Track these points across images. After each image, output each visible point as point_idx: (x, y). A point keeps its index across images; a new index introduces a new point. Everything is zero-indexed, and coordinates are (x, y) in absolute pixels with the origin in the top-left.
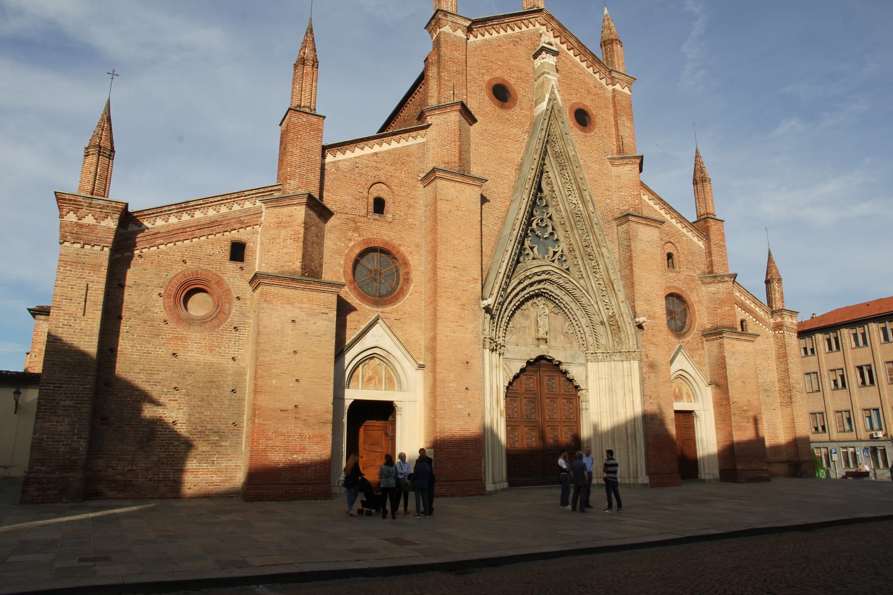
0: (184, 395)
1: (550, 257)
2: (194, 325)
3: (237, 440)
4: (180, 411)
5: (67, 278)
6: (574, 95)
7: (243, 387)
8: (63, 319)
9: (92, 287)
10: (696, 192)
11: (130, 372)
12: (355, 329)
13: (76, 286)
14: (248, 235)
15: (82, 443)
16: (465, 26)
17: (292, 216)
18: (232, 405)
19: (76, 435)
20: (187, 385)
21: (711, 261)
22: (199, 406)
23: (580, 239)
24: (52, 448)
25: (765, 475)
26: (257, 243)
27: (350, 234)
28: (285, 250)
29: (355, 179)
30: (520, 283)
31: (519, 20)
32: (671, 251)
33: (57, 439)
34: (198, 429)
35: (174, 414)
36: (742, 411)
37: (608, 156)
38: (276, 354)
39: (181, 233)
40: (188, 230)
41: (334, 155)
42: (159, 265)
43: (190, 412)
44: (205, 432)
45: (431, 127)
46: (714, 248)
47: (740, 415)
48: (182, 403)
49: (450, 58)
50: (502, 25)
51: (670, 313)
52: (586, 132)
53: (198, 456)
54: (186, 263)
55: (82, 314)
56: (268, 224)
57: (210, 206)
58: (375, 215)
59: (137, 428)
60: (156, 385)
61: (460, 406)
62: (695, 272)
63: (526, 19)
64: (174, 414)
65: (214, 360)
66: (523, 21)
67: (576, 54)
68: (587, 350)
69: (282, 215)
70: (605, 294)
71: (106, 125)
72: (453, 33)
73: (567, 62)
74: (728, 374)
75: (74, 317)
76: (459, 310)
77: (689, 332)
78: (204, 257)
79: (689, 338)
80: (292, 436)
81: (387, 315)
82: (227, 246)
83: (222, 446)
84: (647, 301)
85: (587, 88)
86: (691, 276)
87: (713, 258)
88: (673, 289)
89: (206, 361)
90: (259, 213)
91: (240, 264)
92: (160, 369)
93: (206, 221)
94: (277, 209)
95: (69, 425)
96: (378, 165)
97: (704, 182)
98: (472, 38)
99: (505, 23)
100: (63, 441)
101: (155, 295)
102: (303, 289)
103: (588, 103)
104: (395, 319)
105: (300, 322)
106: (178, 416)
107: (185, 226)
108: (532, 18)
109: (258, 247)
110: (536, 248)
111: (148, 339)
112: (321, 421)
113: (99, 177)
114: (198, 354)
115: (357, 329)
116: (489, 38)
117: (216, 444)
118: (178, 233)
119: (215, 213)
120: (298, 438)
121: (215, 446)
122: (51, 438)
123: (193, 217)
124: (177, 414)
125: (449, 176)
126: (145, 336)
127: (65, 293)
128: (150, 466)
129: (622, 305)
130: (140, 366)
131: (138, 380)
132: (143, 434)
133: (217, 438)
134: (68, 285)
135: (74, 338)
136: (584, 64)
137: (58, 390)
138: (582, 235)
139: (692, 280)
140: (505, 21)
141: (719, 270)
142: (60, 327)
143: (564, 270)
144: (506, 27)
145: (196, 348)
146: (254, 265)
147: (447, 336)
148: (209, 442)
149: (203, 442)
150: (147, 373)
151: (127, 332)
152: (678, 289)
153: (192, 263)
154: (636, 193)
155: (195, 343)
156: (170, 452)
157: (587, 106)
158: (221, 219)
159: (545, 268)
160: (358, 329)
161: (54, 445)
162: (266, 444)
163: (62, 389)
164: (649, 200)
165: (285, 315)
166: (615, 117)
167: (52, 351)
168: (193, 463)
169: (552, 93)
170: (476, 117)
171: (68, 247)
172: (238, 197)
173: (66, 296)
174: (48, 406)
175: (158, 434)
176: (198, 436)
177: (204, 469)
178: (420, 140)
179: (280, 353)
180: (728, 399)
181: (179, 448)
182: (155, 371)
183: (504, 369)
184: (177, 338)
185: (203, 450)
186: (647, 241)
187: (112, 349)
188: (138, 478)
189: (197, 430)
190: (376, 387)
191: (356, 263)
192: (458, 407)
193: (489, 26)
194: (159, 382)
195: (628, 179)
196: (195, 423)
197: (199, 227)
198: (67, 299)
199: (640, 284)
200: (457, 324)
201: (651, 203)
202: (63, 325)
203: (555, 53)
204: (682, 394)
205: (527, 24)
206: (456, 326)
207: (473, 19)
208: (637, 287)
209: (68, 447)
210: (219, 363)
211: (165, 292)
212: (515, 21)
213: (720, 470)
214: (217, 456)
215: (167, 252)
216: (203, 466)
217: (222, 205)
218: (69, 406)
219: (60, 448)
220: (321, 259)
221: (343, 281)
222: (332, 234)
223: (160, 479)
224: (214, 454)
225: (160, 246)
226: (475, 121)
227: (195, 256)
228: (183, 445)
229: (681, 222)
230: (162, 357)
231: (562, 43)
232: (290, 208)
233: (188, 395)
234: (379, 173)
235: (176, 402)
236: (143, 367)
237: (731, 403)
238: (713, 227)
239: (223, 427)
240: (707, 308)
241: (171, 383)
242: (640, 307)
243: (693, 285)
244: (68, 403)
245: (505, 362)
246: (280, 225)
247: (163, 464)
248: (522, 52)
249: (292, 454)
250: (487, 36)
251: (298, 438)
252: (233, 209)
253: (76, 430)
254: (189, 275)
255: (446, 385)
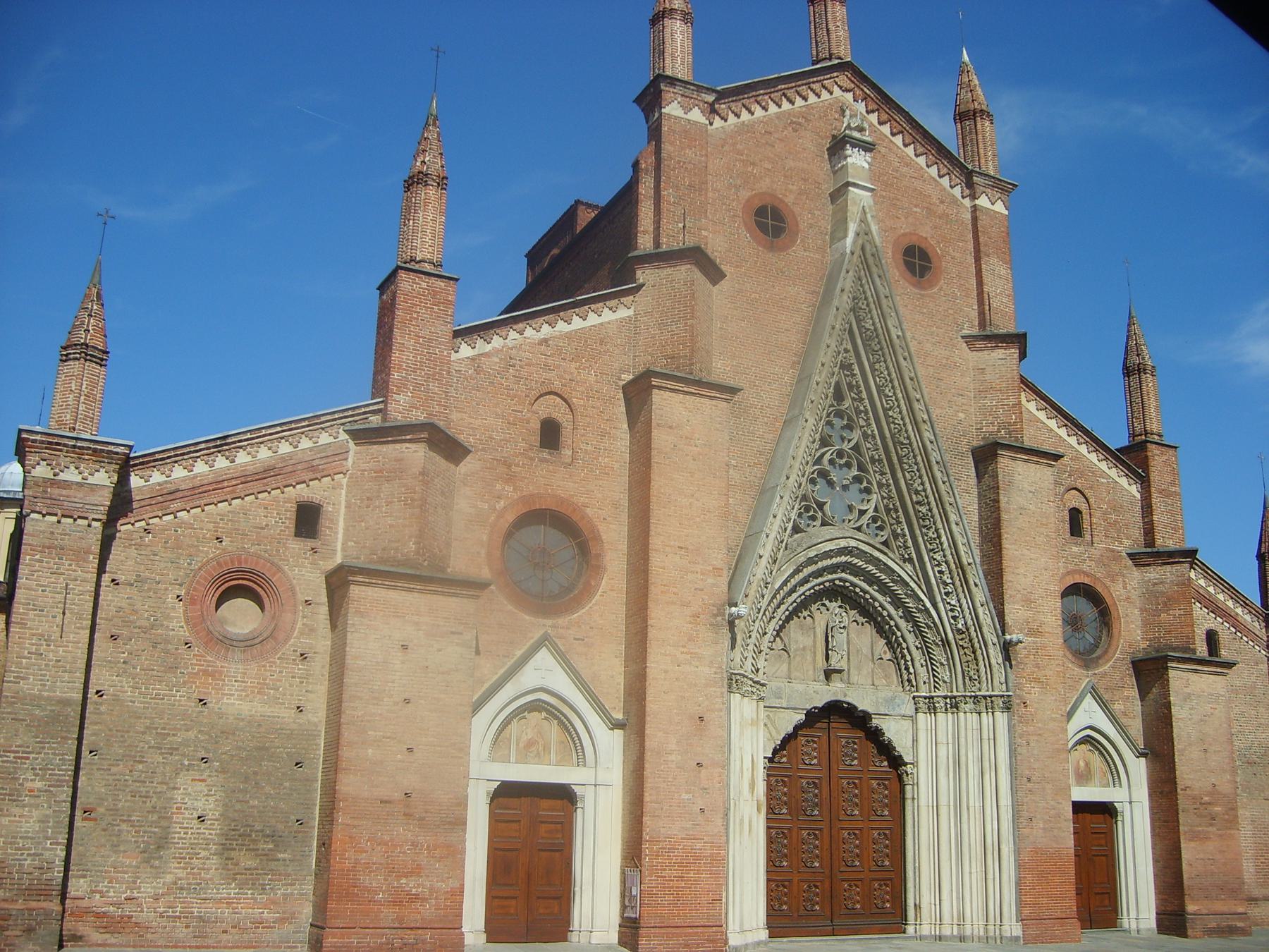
0: (216, 771)
1: (852, 522)
2: (234, 651)
3: (303, 849)
4: (211, 799)
5: (36, 574)
6: (903, 219)
7: (314, 758)
8: (29, 644)
9: (74, 589)
10: (1129, 391)
11: (128, 732)
12: (505, 656)
13: (50, 587)
14: (324, 491)
15: (59, 852)
16: (706, 103)
17: (402, 460)
18: (295, 790)
19: (48, 838)
20: (222, 754)
21: (1152, 522)
22: (241, 791)
23: (909, 490)
24: (12, 860)
25: (1240, 924)
26: (340, 504)
27: (498, 487)
28: (389, 521)
29: (508, 388)
30: (797, 571)
31: (803, 85)
32: (1076, 505)
33: (21, 845)
34: (239, 830)
35: (199, 804)
36: (1200, 803)
37: (964, 331)
38: (374, 704)
39: (213, 490)
40: (226, 484)
41: (473, 345)
42: (178, 546)
43: (227, 800)
44: (250, 836)
45: (644, 288)
46: (1156, 499)
47: (1195, 811)
48: (212, 786)
49: (679, 162)
50: (772, 96)
51: (1072, 622)
52: (923, 288)
53: (238, 876)
54: (221, 542)
55: (58, 634)
56: (359, 473)
57: (261, 443)
58: (542, 452)
59: (141, 826)
60: (171, 754)
61: (685, 796)
62: (1121, 543)
63: (817, 81)
64: (199, 804)
65: (267, 710)
66: (812, 85)
67: (907, 141)
68: (917, 691)
69: (384, 458)
70: (950, 590)
71: (95, 307)
72: (685, 116)
73: (892, 158)
74: (1175, 736)
75: (45, 640)
76: (688, 625)
77: (1106, 657)
78: (251, 532)
79: (1106, 668)
80: (399, 845)
81: (561, 631)
82: (290, 511)
83: (278, 860)
84: (1028, 602)
85: (927, 205)
86: (1113, 551)
87: (1155, 518)
88: (1078, 576)
89: (253, 713)
90: (343, 454)
91: (310, 543)
92: (178, 726)
93: (254, 468)
94: (375, 446)
95: (39, 821)
96: (550, 362)
97: (1142, 374)
98: (718, 122)
99: (777, 91)
100: (30, 849)
101: (171, 598)
102: (420, 591)
103: (927, 233)
104: (575, 639)
105: (415, 648)
106: (207, 807)
107: (221, 479)
108: (827, 79)
109: (343, 510)
110: (828, 504)
111: (159, 674)
112: (448, 820)
113: (85, 399)
114: (241, 700)
115: (508, 657)
116: (749, 121)
117: (268, 857)
118: (209, 491)
119: (270, 453)
120: (408, 849)
121: (267, 860)
122: (11, 843)
123: (233, 461)
124: (204, 804)
125: (674, 385)
126: (153, 670)
127: (33, 600)
128: (161, 891)
129: (980, 610)
130: (146, 721)
131: (142, 744)
132: (151, 837)
133: (271, 846)
134: (37, 585)
135: (45, 675)
136: (922, 161)
137: (21, 763)
138: (911, 482)
139: (1115, 556)
140: (779, 87)
141: (1166, 540)
142: (25, 658)
143: (878, 546)
144: (781, 99)
145: (237, 690)
146: (333, 544)
147: (666, 672)
148: (257, 852)
149: (247, 853)
150: (157, 733)
151: (124, 662)
152: (1088, 576)
153: (231, 542)
154: (1012, 401)
155: (235, 681)
156: (192, 869)
157: (926, 239)
158: (280, 465)
159: (843, 543)
160: (511, 656)
161: (17, 854)
162: (356, 859)
163: (27, 761)
164: (1038, 410)
165: (390, 636)
166: (978, 259)
167: (12, 697)
168: (231, 889)
169: (863, 221)
170: (723, 268)
171: (37, 520)
172: (308, 426)
173: (33, 605)
174: (6, 789)
175: (175, 838)
176: (240, 842)
177: (247, 899)
178: (623, 313)
179: (381, 703)
180: (1173, 781)
181: (208, 862)
182: (169, 729)
183: (765, 725)
184: (206, 673)
185: (246, 867)
186: (1030, 492)
187: (101, 691)
188: (142, 911)
189: (237, 832)
190: (539, 757)
191: (509, 535)
192: (682, 797)
193: (748, 98)
194: (177, 749)
195: (997, 376)
196: (234, 820)
197: (243, 479)
198: (36, 610)
199: (1016, 571)
200: (685, 650)
201: (1042, 415)
202: (29, 653)
203: (868, 147)
204: (1090, 771)
205: (818, 91)
206: (682, 653)
207: (719, 88)
208: (1007, 577)
209: (37, 858)
210: (274, 717)
211: (187, 593)
212: (795, 86)
213: (1157, 914)
214: (270, 877)
215: (191, 524)
216: (247, 894)
217: (283, 441)
218: (39, 790)
219: (26, 860)
220: (448, 532)
221: (485, 574)
222: (468, 489)
223: (178, 914)
224: (265, 874)
225: (179, 514)
226: (722, 275)
227: (235, 529)
228: (215, 857)
229: (1097, 450)
230: (182, 706)
231: (881, 123)
232: (398, 446)
233: (223, 771)
234: (551, 375)
235: (203, 784)
236: (150, 724)
237: (1179, 790)
238: (1158, 459)
239: (281, 826)
240: (1143, 610)
241: (197, 751)
242: (1014, 612)
243: (1116, 568)
244: (38, 784)
245: (767, 713)
246: (381, 475)
247: (182, 889)
248: (812, 145)
249: (399, 877)
250: (745, 116)
251: (408, 849)
252: (301, 447)
253: (50, 830)
254: (226, 564)
255: (663, 759)
